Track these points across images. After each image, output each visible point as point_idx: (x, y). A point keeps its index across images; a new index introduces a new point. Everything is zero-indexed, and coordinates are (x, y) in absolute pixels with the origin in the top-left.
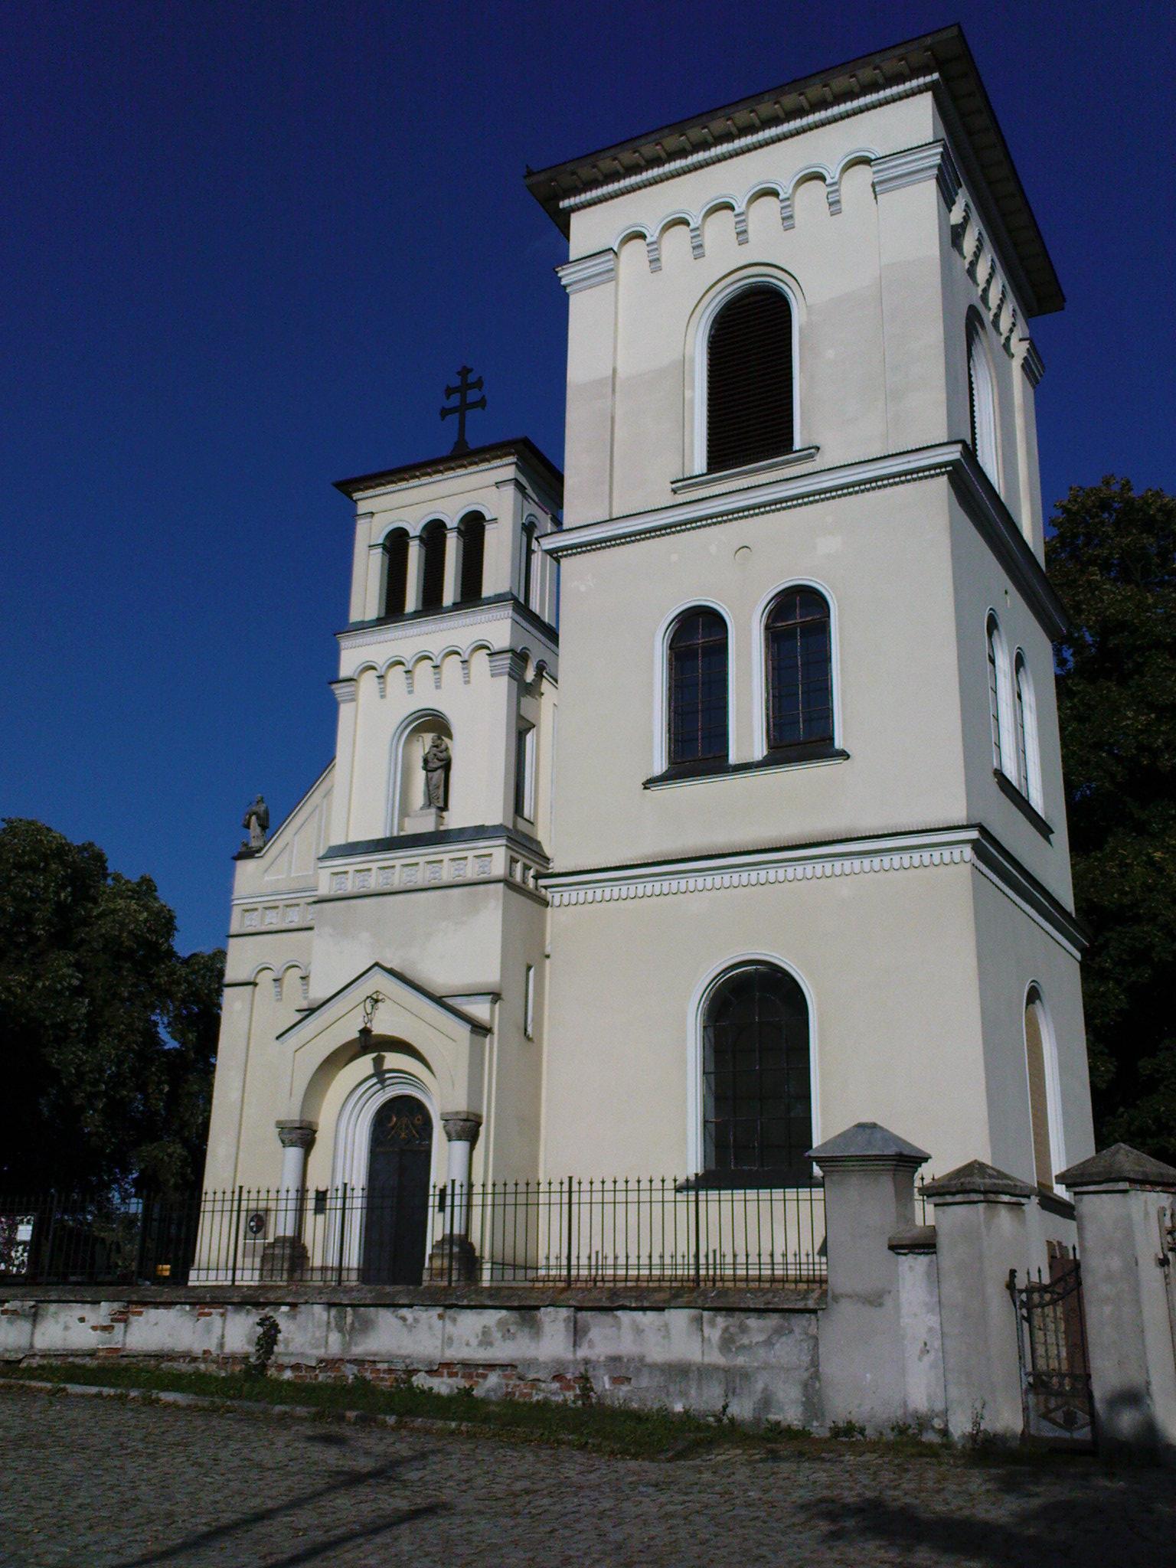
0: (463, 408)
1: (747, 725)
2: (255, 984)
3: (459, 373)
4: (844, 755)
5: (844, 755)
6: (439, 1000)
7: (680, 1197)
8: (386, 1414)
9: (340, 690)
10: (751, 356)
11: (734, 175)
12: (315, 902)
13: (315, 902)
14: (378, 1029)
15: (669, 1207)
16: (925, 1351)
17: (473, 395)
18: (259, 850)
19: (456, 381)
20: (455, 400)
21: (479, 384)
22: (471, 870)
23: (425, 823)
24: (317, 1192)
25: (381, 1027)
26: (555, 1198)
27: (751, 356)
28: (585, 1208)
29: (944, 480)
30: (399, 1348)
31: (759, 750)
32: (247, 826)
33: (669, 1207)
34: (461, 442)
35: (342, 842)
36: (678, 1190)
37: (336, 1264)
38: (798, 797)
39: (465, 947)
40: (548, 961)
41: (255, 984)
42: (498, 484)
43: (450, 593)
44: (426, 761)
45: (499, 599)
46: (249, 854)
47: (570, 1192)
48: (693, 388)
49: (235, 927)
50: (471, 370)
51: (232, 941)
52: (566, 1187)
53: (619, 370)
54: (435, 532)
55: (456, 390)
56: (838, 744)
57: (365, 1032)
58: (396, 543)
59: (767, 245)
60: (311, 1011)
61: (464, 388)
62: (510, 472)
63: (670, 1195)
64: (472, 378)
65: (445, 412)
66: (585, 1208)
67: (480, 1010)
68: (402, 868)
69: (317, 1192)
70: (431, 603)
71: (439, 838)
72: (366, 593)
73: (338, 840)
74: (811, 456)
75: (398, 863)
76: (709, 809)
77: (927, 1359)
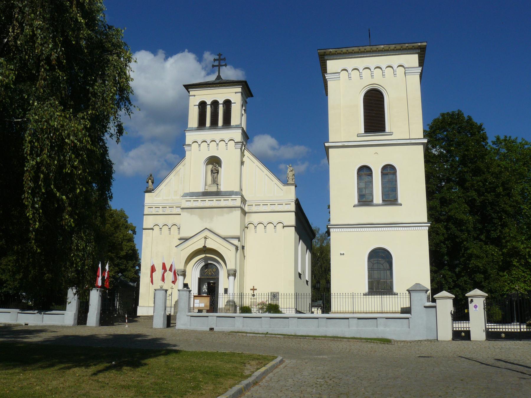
1: (378, 196)
2: (153, 229)
4: (401, 205)
5: (401, 205)
6: (224, 239)
7: (365, 296)
9: (186, 148)
10: (374, 106)
11: (372, 61)
14: (208, 246)
15: (362, 299)
18: (153, 190)
20: (216, 63)
22: (230, 203)
23: (214, 189)
25: (209, 245)
26: (350, 297)
27: (374, 106)
29: (422, 146)
31: (381, 202)
32: (148, 182)
33: (362, 299)
34: (219, 77)
35: (188, 192)
36: (364, 295)
38: (388, 214)
39: (228, 223)
41: (153, 229)
42: (236, 93)
43: (208, 124)
44: (212, 171)
45: (237, 127)
46: (150, 191)
49: (145, 213)
54: (215, 104)
56: (400, 201)
57: (205, 247)
58: (202, 105)
59: (377, 80)
60: (186, 239)
62: (239, 90)
63: (362, 296)
67: (236, 242)
68: (208, 202)
70: (214, 123)
71: (218, 194)
73: (187, 191)
74: (391, 135)
75: (207, 199)
76: (367, 214)
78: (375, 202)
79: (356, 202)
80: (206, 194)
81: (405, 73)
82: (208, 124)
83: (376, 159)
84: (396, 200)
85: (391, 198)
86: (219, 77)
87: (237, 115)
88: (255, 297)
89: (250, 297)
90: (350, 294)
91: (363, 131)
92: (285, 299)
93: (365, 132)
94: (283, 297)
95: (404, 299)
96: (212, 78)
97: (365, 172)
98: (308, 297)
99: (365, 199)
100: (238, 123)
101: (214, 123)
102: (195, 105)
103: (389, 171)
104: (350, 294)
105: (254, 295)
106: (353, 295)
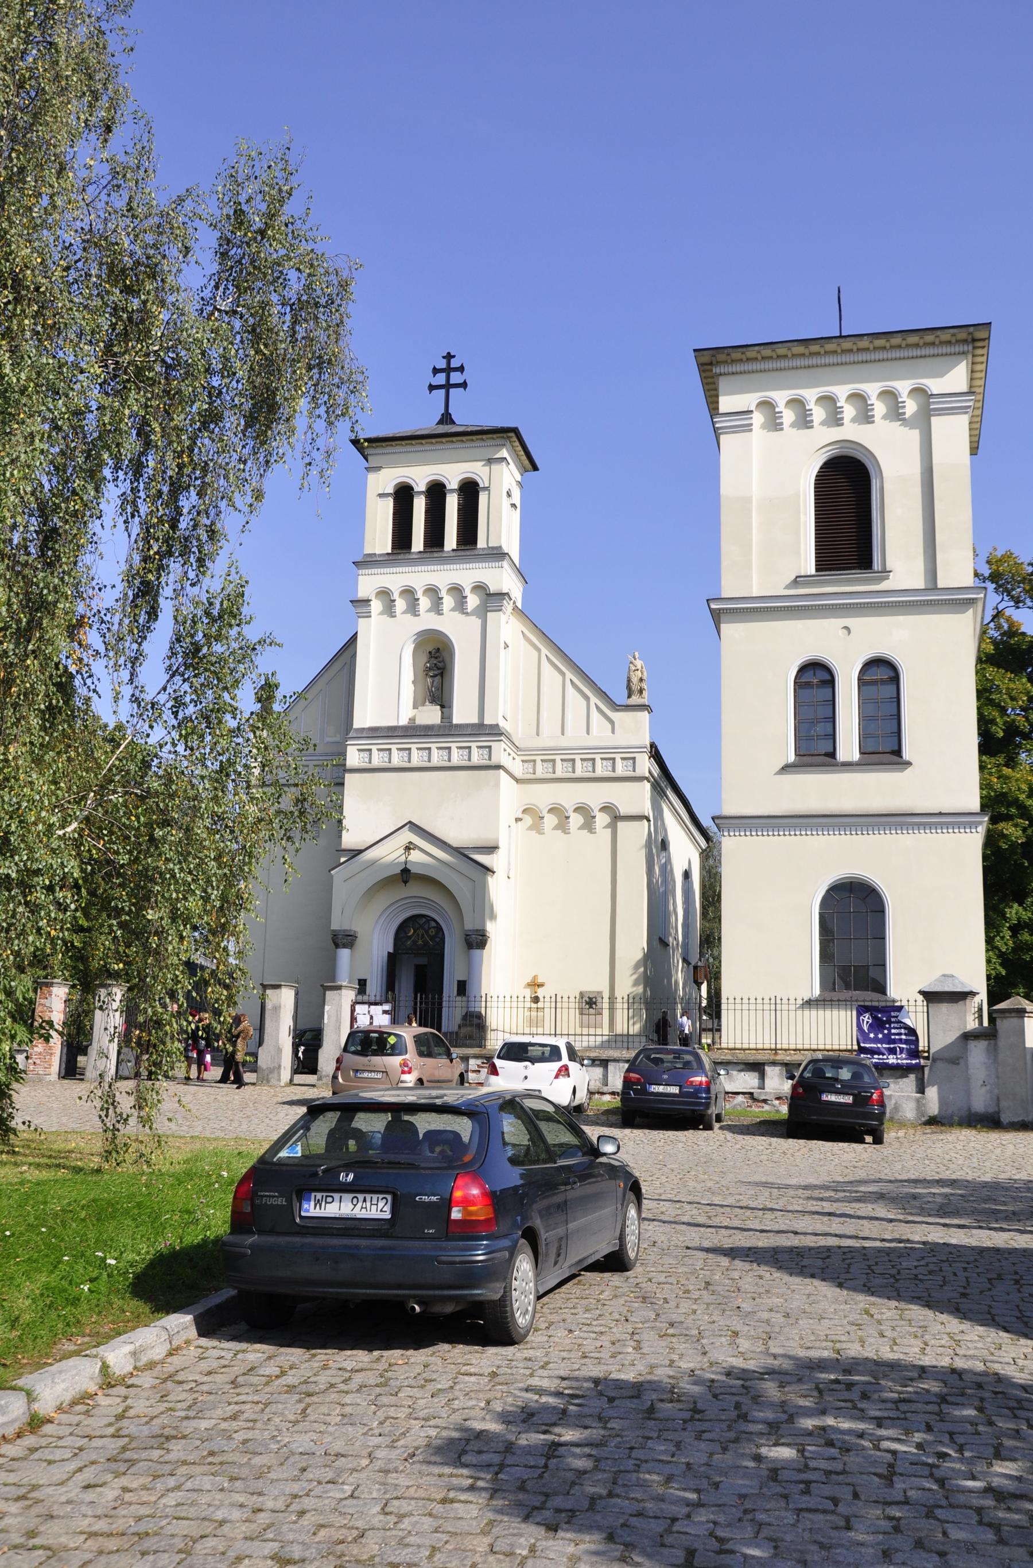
0: (448, 386)
4: (909, 764)
12: (732, 1253)
13: (732, 1253)
16: (984, 1084)
17: (456, 378)
19: (442, 364)
21: (461, 369)
26: (767, 1007)
28: (785, 1013)
31: (856, 756)
37: (937, 423)
40: (344, 954)
43: (451, 540)
48: (357, 1247)
51: (347, 775)
54: (436, 492)
56: (907, 754)
61: (448, 370)
64: (454, 363)
65: (432, 388)
66: (785, 1013)
70: (435, 537)
72: (380, 536)
77: (984, 1089)
78: (842, 755)
79: (792, 758)
80: (412, 731)
81: (715, 430)
82: (451, 540)
83: (846, 645)
84: (898, 752)
85: (885, 747)
86: (446, 418)
87: (502, 522)
88: (540, 1005)
89: (528, 1005)
90: (767, 1001)
91: (811, 569)
92: (760, 1013)
93: (817, 570)
94: (565, 1005)
95: (508, 1010)
96: (429, 423)
97: (883, 674)
98: (572, 1005)
99: (815, 749)
101: (435, 537)
102: (381, 495)
103: (882, 675)
104: (767, 1001)
105: (536, 1000)
106: (775, 1003)
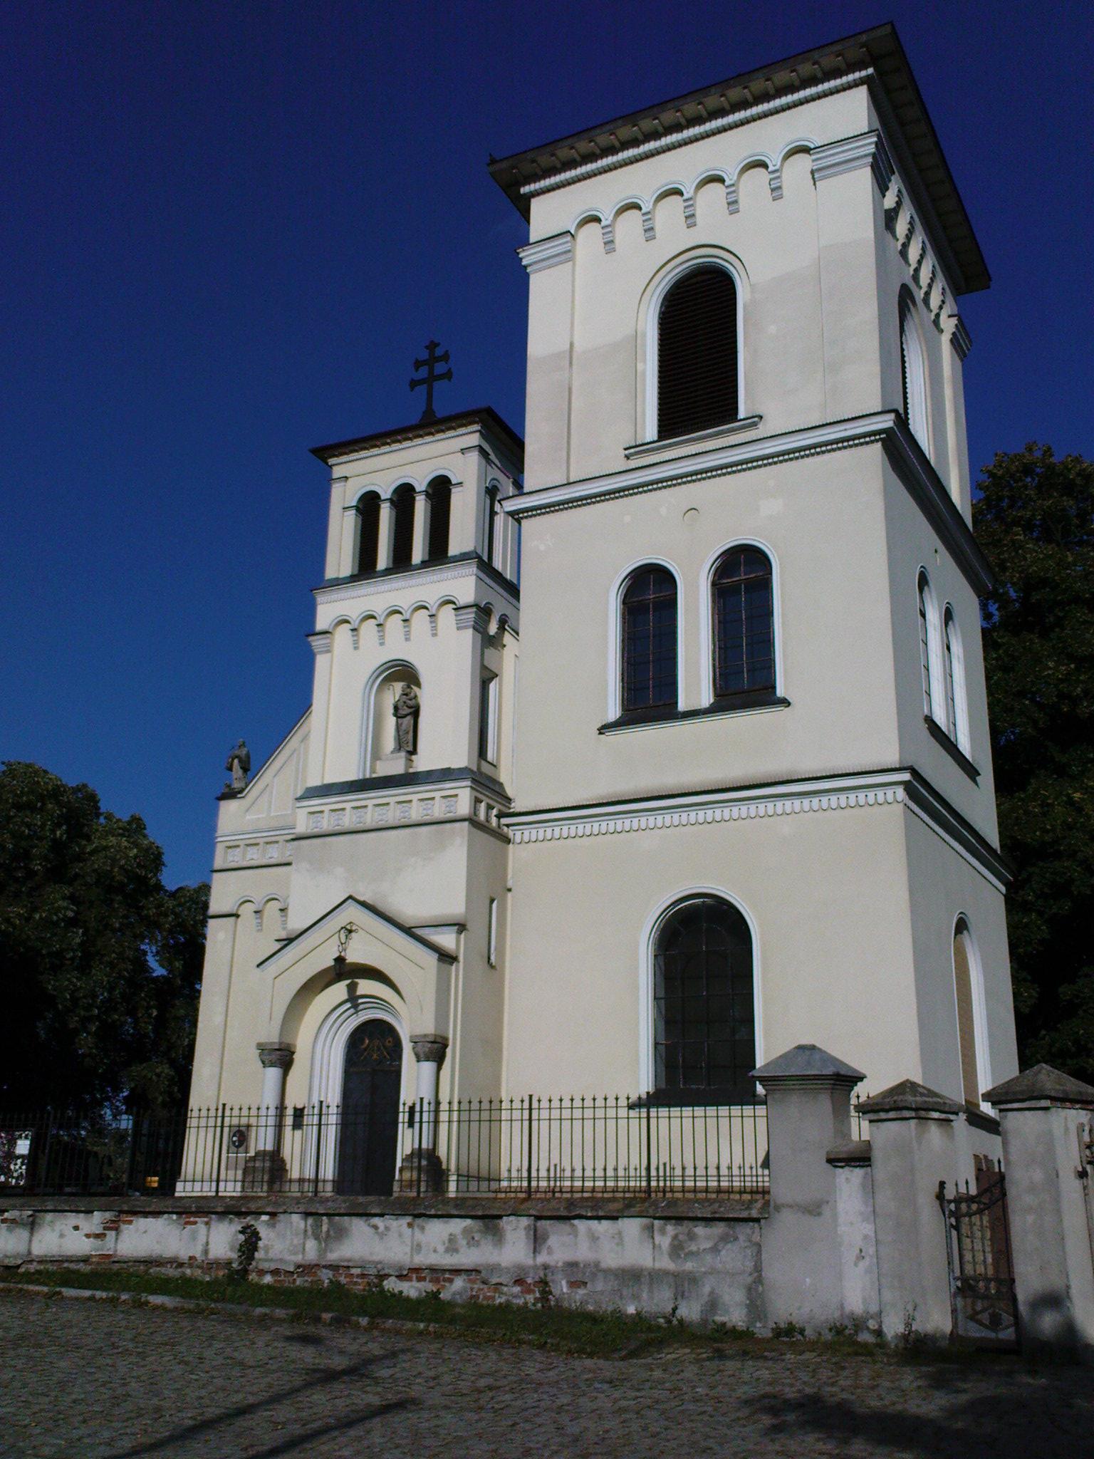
0: (430, 380)
1: (695, 675)
2: (237, 916)
3: (427, 347)
4: (785, 702)
5: (785, 702)
6: (408, 931)
7: (633, 1113)
8: (359, 1315)
9: (316, 642)
10: (699, 331)
11: (682, 163)
12: (293, 840)
13: (293, 840)
14: (352, 957)
15: (622, 1123)
16: (861, 1257)
17: (440, 368)
18: (241, 791)
19: (424, 355)
20: (423, 372)
21: (446, 357)
22: (438, 810)
24: (295, 1109)
25: (355, 955)
26: (516, 1114)
27: (699, 331)
28: (544, 1124)
29: (878, 446)
30: (371, 1254)
31: (706, 698)
32: (230, 769)
33: (622, 1123)
35: (318, 783)
36: (630, 1107)
38: (742, 742)
39: (433, 881)
41: (237, 916)
42: (463, 451)
43: (419, 552)
44: (396, 708)
45: (464, 557)
46: (231, 794)
47: (530, 1109)
49: (218, 863)
50: (438, 345)
51: (216, 875)
52: (526, 1105)
53: (576, 345)
54: (404, 495)
55: (424, 363)
56: (780, 692)
57: (340, 960)
58: (368, 505)
59: (713, 228)
60: (289, 941)
61: (431, 361)
62: (474, 439)
63: (623, 1112)
64: (439, 352)
65: (414, 384)
66: (544, 1124)
67: (447, 940)
68: (374, 808)
69: (295, 1109)
70: (401, 561)
71: (409, 779)
72: (340, 552)
73: (314, 781)
74: (755, 424)
75: (370, 803)
76: (659, 753)
77: (863, 1265)
100: (468, 546)
